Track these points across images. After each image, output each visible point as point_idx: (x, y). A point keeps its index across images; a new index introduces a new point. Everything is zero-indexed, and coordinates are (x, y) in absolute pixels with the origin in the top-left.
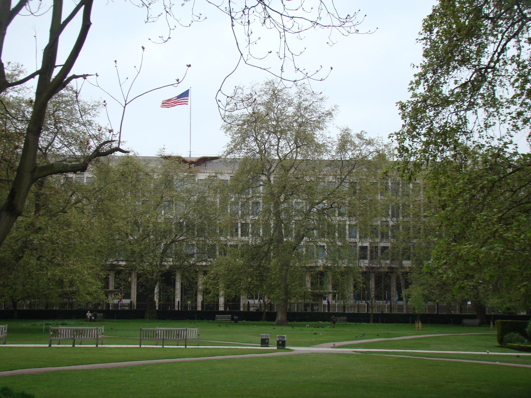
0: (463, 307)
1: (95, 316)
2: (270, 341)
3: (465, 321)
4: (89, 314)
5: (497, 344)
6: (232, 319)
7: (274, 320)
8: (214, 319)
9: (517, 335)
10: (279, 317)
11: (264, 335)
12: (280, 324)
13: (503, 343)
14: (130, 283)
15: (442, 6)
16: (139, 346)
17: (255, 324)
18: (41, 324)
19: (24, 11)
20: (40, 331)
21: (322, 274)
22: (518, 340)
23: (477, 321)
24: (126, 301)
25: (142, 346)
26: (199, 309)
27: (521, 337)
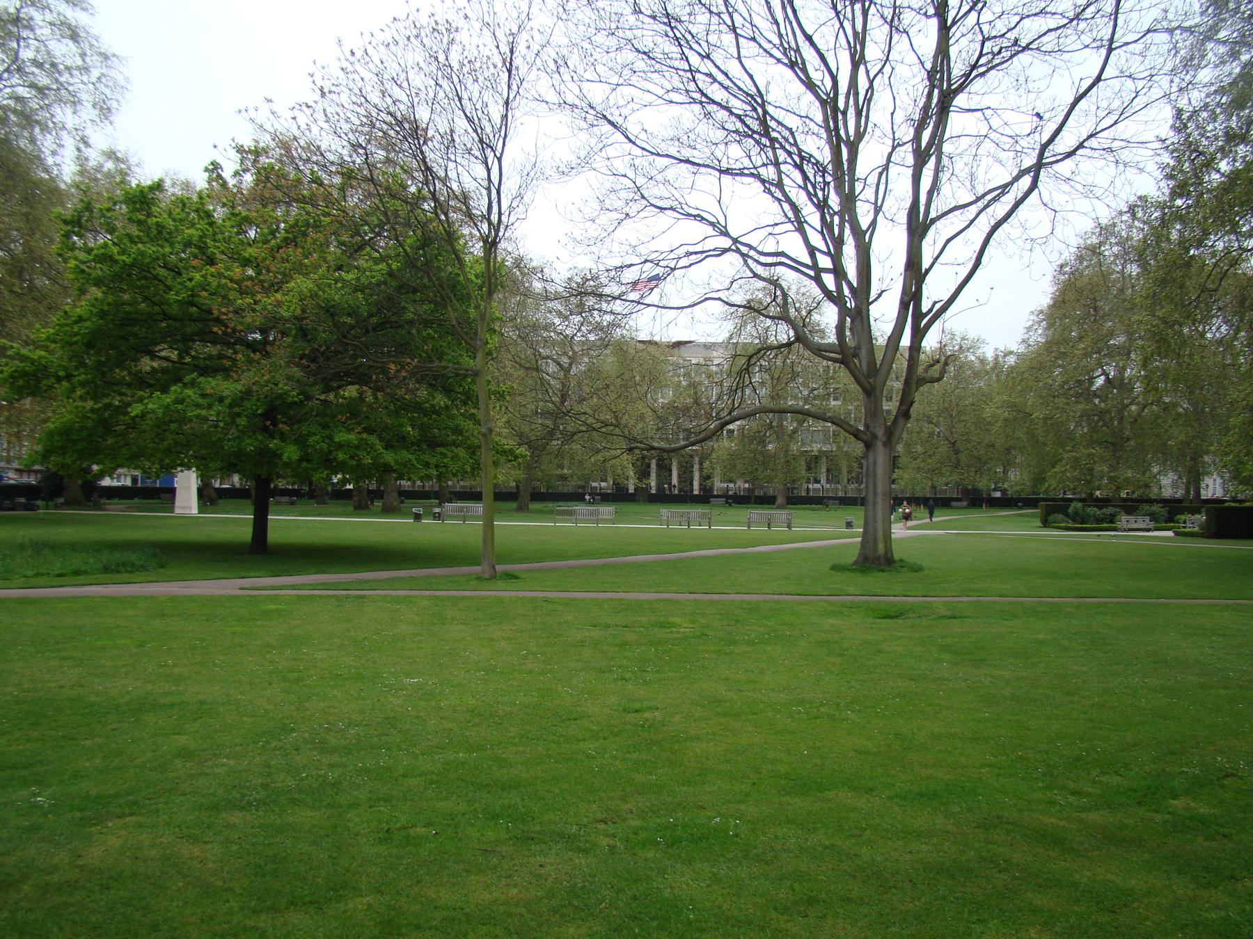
0: (507, 476)
1: (594, 499)
2: (855, 522)
3: (954, 504)
4: (587, 497)
5: (1040, 524)
6: (727, 503)
7: (774, 503)
8: (708, 502)
9: (1061, 516)
10: (780, 500)
11: (849, 518)
12: (780, 507)
13: (1046, 523)
14: (649, 466)
15: (1249, 279)
16: (928, 520)
17: (805, 509)
18: (564, 506)
19: (519, 114)
20: (551, 512)
21: (816, 457)
22: (1063, 521)
23: (965, 503)
24: (604, 484)
25: (934, 519)
26: (696, 492)
27: (1065, 518)
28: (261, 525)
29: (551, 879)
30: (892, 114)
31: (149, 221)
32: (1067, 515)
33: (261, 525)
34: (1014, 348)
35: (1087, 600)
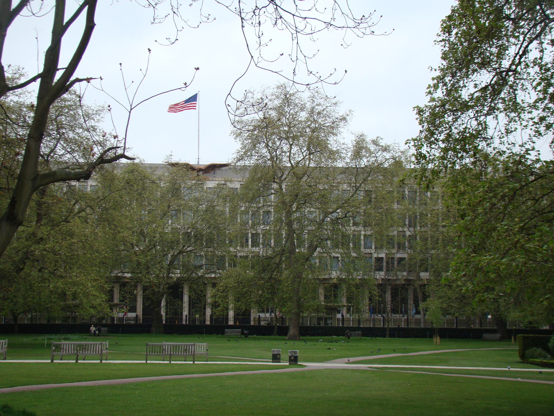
1: (99, 330)
2: (282, 356)
3: (485, 336)
4: (93, 329)
5: (519, 359)
6: (243, 333)
7: (286, 334)
8: (223, 333)
10: (292, 331)
11: (276, 350)
13: (524, 359)
16: (145, 362)
18: (43, 339)
20: (42, 346)
22: (540, 356)
23: (498, 336)
24: (132, 315)
25: (148, 362)
26: (208, 323)
27: (543, 352)
28: (146, 362)
29: (440, 242)
30: (265, 7)
31: (135, 247)
32: (547, 349)
33: (146, 362)
34: (485, 71)
35: (467, 376)
